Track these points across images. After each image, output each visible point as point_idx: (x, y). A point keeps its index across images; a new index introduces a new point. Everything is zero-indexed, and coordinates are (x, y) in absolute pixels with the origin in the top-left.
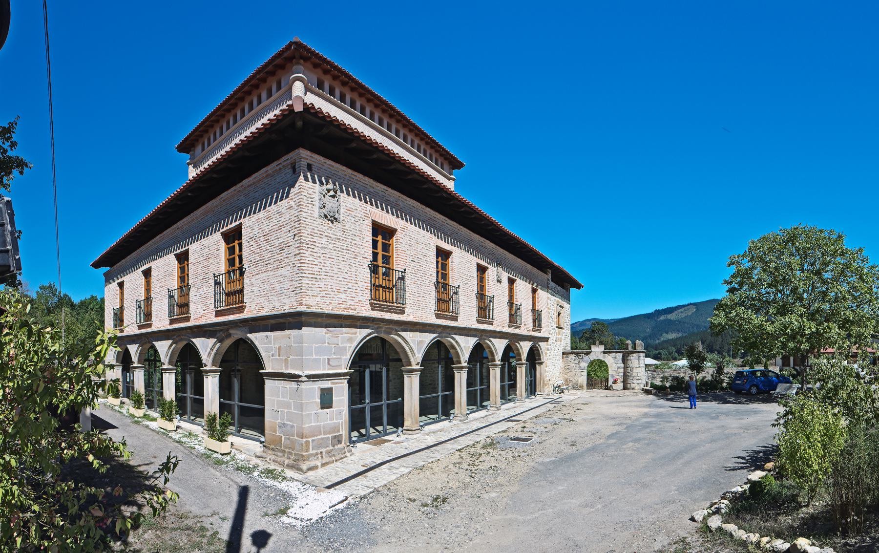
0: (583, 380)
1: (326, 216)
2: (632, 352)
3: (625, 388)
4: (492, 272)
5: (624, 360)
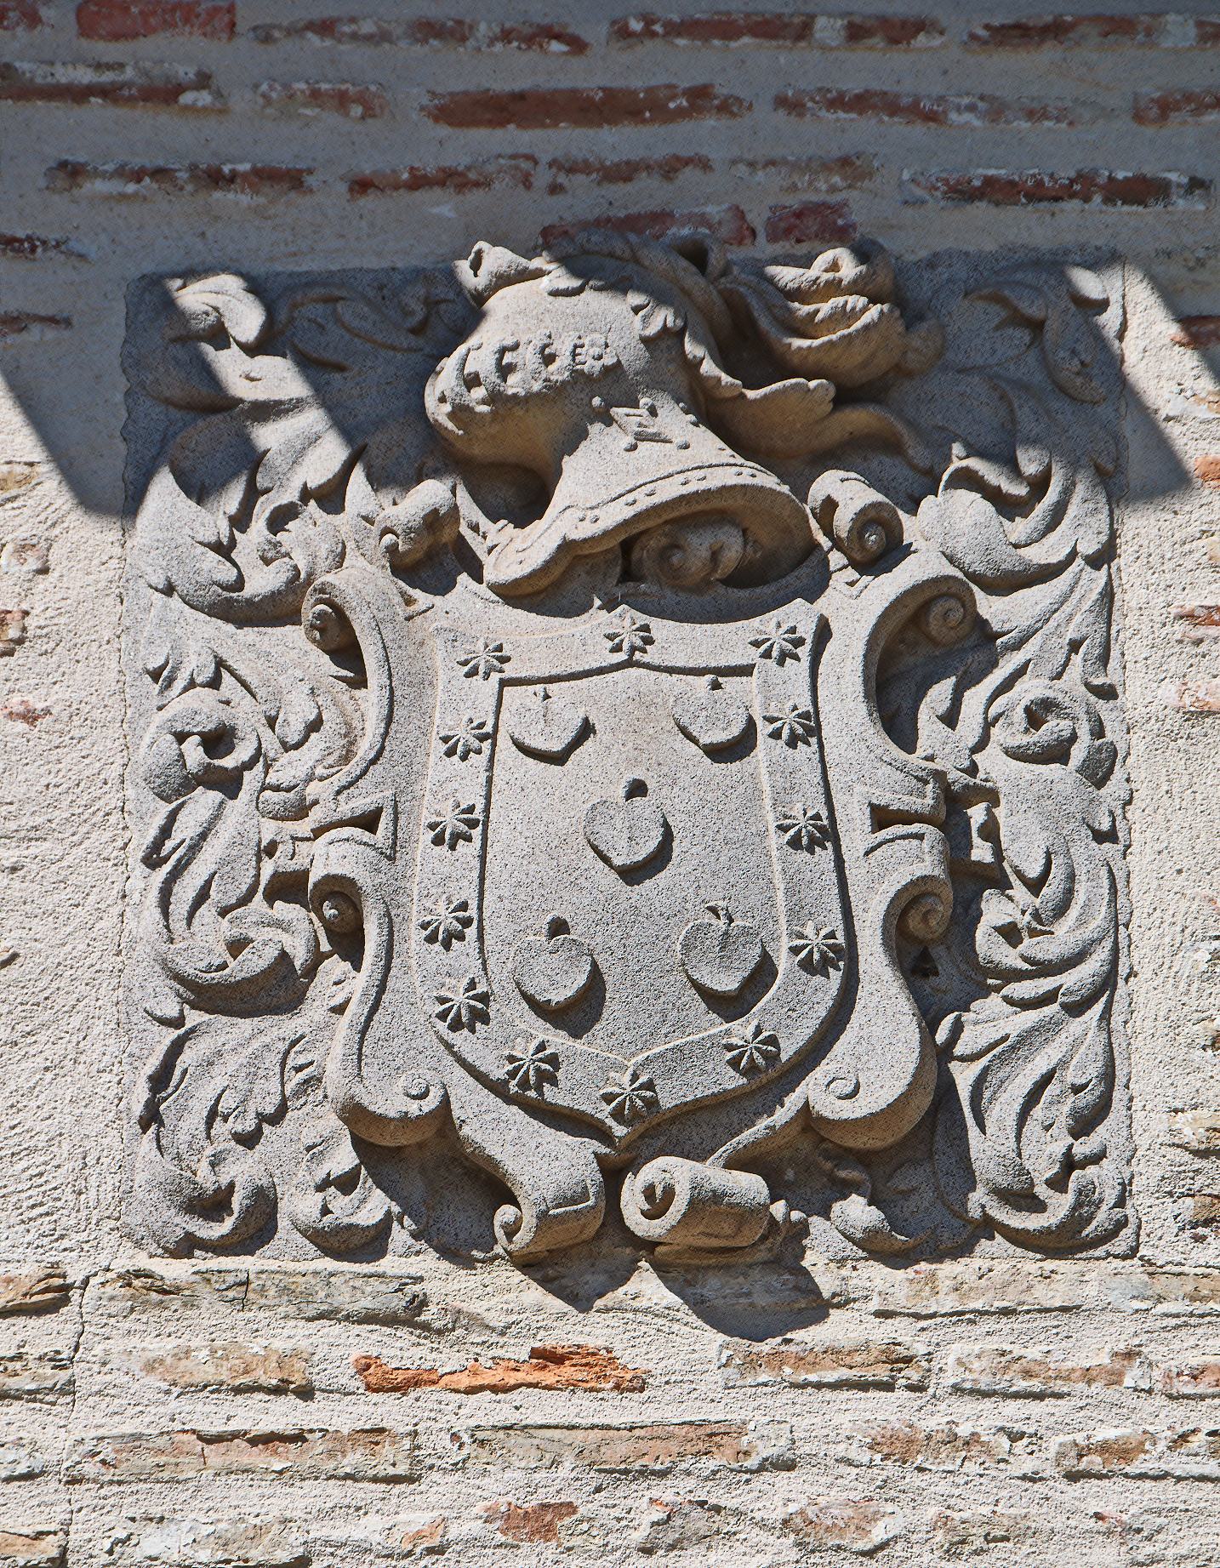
1: (434, 1177)
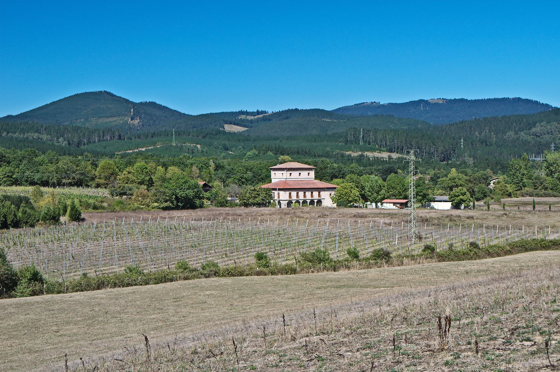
4: (307, 193)
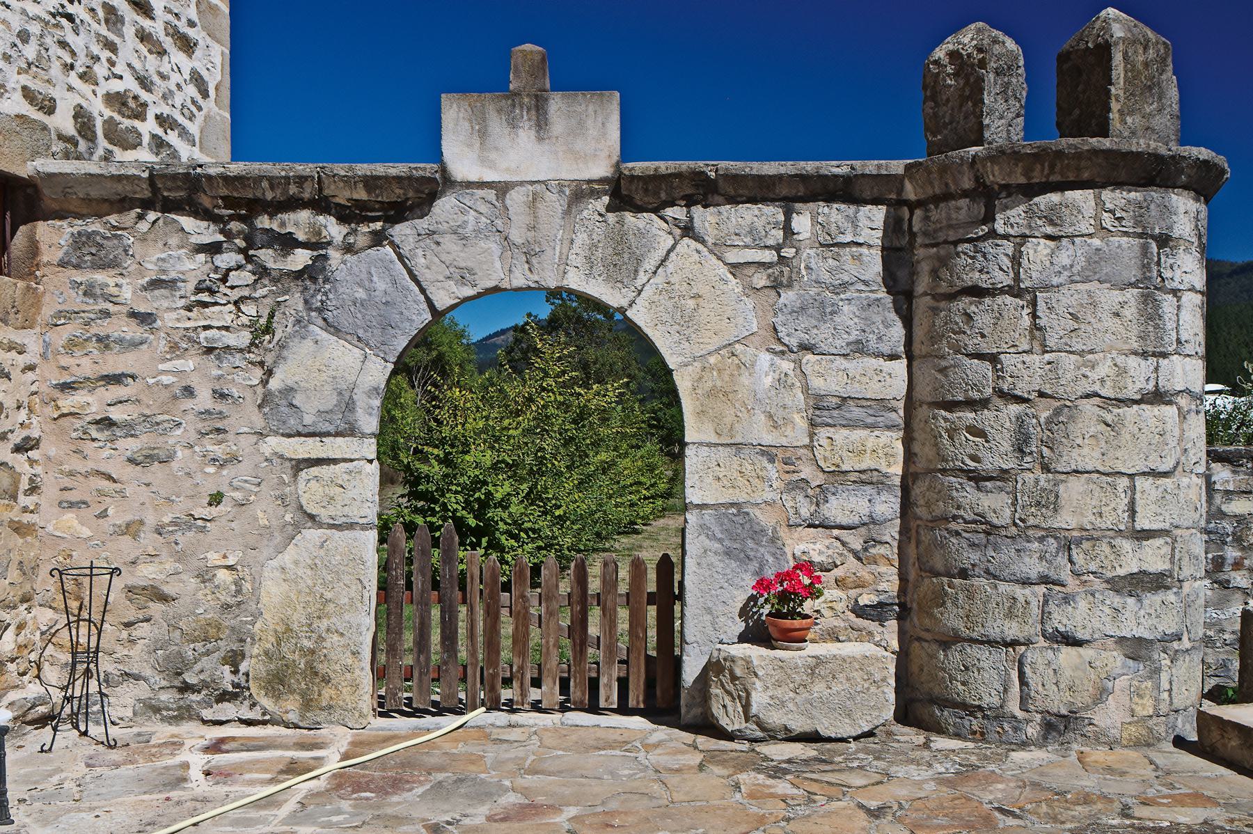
0: (317, 560)
2: (1043, 174)
3: (919, 704)
5: (913, 278)
